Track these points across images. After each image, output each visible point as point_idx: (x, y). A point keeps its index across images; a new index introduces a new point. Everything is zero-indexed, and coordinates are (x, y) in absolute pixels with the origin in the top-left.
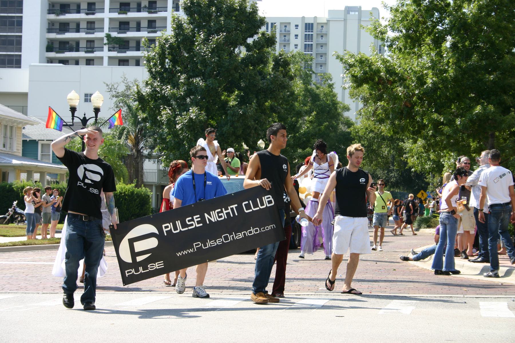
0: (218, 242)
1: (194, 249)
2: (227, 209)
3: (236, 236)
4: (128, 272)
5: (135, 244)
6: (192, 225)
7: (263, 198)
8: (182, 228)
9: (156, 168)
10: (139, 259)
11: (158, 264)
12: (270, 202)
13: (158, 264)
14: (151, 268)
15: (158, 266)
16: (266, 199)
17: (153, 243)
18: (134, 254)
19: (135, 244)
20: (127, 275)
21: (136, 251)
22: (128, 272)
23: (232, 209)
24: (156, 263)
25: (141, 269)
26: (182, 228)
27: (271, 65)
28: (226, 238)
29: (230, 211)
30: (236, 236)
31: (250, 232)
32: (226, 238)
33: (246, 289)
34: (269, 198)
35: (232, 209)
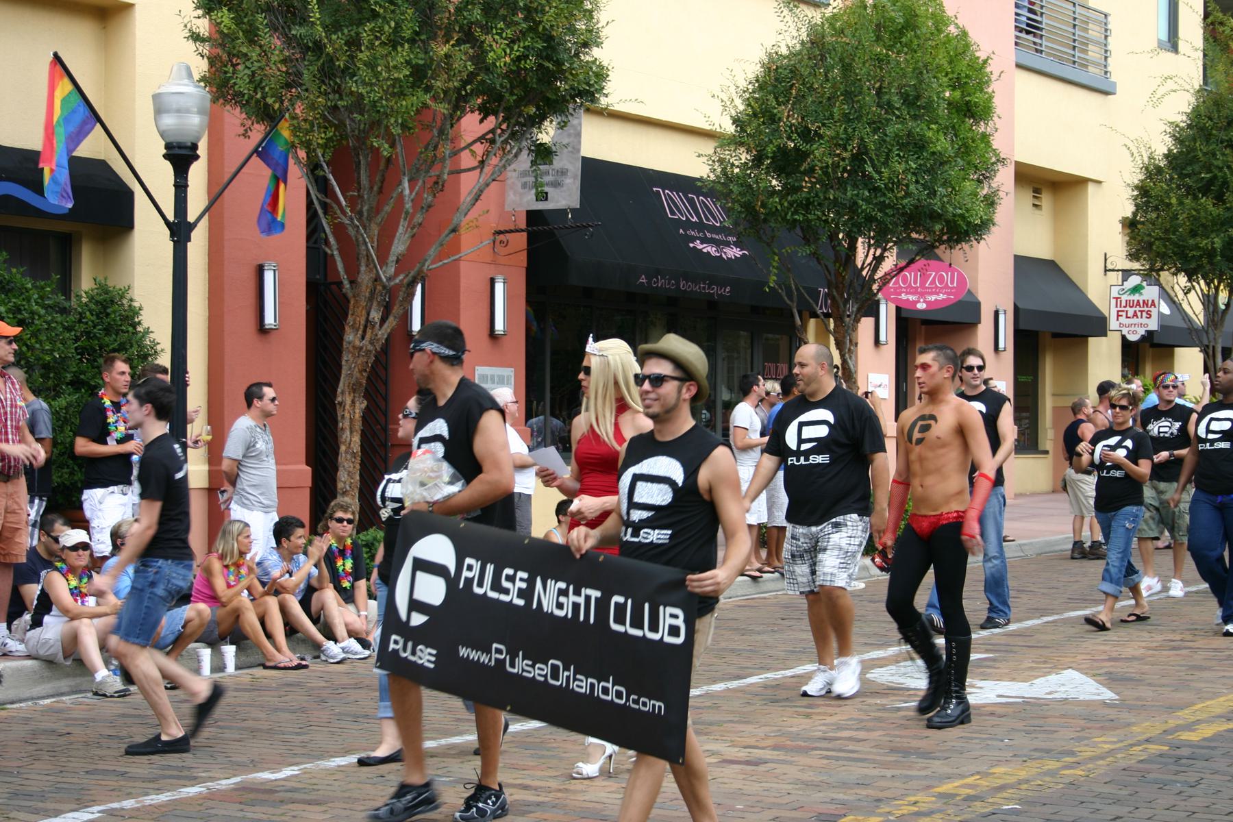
0: (539, 672)
1: (490, 660)
2: (577, 593)
3: (575, 679)
6: (506, 592)
7: (661, 608)
12: (674, 631)
16: (667, 615)
17: (823, 431)
19: (640, 485)
23: (588, 598)
25: (802, 458)
28: (555, 673)
29: (581, 600)
30: (575, 679)
31: (605, 691)
32: (555, 673)
34: (676, 617)
35: (588, 598)
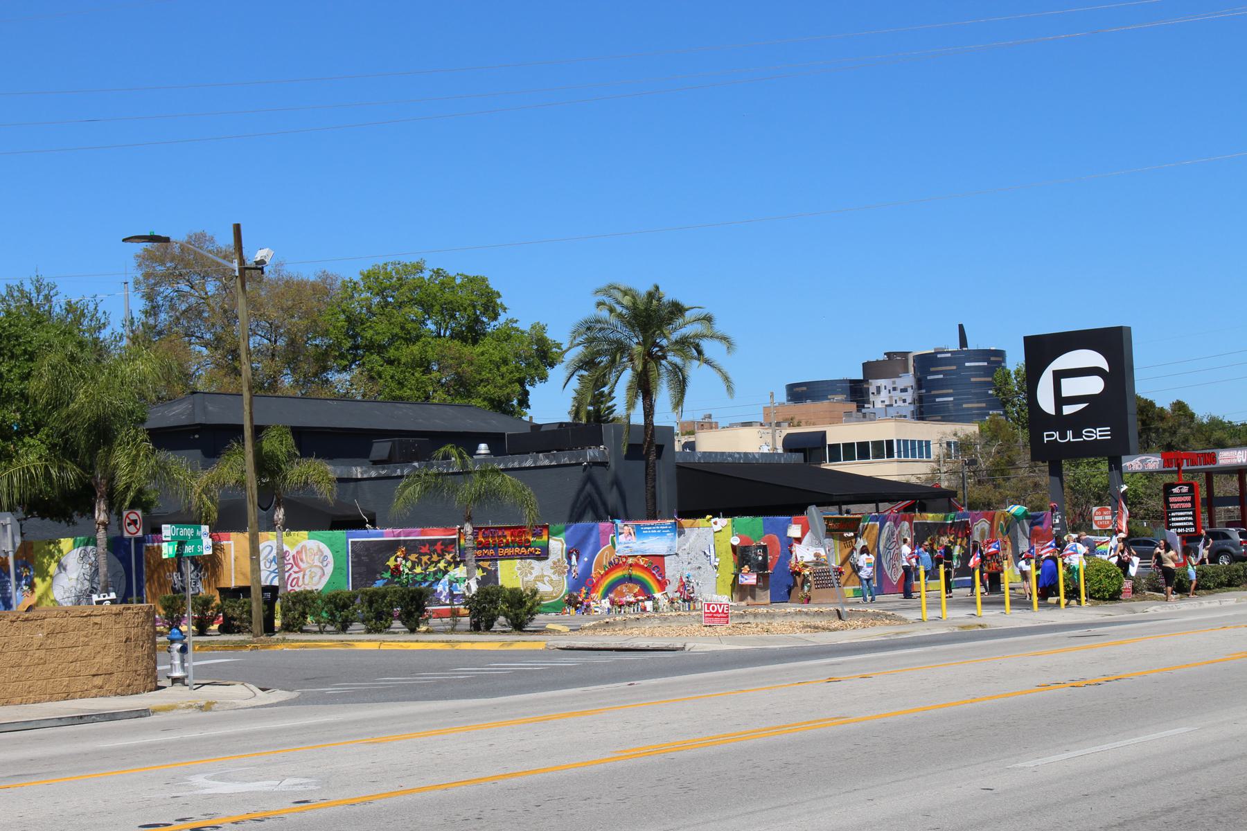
4: (1048, 436)
5: (1064, 382)
10: (1068, 410)
14: (1086, 436)
18: (1060, 401)
20: (1046, 439)
22: (1048, 436)
24: (1098, 429)
25: (1070, 434)
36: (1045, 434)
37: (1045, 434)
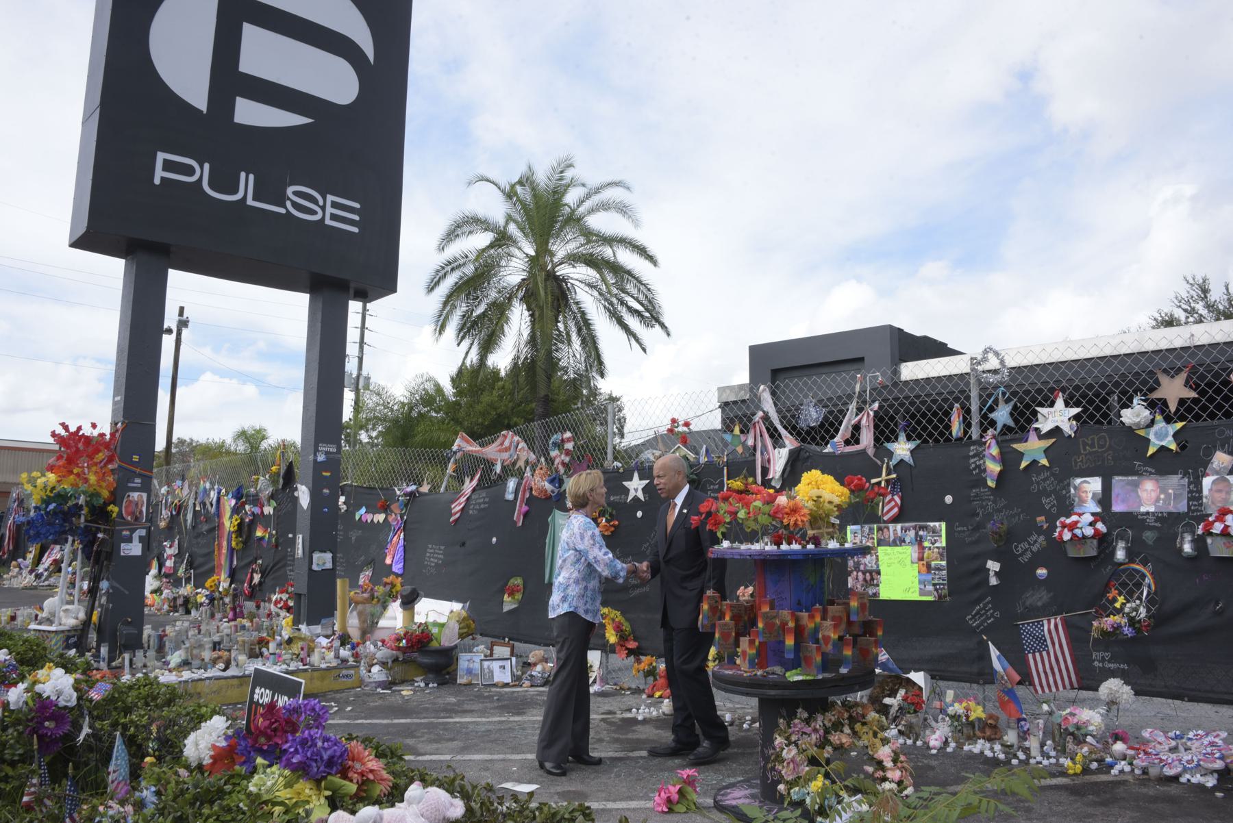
4: (168, 165)
8: (255, 199)
9: (357, 355)
10: (249, 112)
11: (334, 205)
13: (334, 205)
14: (295, 205)
15: (333, 217)
20: (159, 174)
21: (172, 273)
22: (168, 165)
24: (330, 198)
25: (247, 183)
26: (255, 199)
27: (33, 511)
33: (581, 202)
36: (161, 157)
37: (161, 157)
